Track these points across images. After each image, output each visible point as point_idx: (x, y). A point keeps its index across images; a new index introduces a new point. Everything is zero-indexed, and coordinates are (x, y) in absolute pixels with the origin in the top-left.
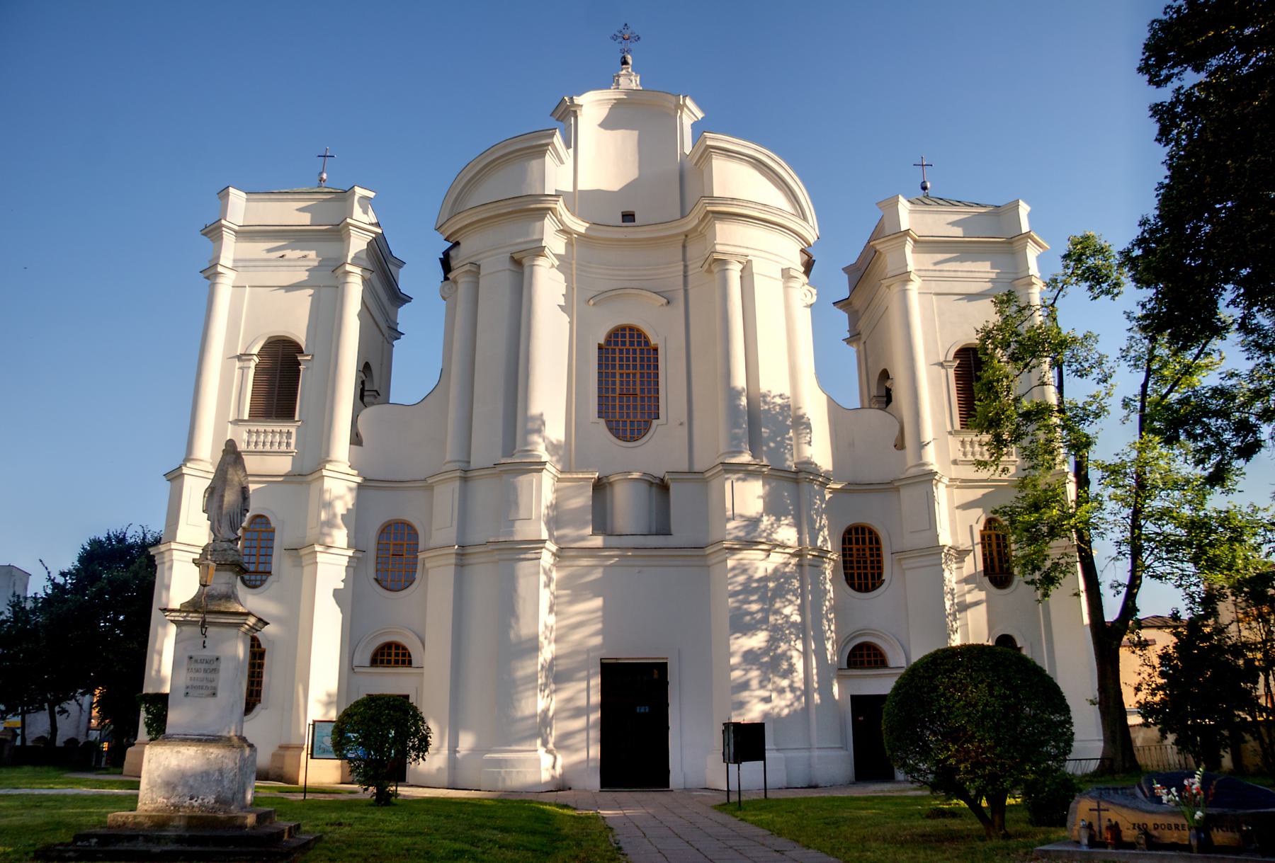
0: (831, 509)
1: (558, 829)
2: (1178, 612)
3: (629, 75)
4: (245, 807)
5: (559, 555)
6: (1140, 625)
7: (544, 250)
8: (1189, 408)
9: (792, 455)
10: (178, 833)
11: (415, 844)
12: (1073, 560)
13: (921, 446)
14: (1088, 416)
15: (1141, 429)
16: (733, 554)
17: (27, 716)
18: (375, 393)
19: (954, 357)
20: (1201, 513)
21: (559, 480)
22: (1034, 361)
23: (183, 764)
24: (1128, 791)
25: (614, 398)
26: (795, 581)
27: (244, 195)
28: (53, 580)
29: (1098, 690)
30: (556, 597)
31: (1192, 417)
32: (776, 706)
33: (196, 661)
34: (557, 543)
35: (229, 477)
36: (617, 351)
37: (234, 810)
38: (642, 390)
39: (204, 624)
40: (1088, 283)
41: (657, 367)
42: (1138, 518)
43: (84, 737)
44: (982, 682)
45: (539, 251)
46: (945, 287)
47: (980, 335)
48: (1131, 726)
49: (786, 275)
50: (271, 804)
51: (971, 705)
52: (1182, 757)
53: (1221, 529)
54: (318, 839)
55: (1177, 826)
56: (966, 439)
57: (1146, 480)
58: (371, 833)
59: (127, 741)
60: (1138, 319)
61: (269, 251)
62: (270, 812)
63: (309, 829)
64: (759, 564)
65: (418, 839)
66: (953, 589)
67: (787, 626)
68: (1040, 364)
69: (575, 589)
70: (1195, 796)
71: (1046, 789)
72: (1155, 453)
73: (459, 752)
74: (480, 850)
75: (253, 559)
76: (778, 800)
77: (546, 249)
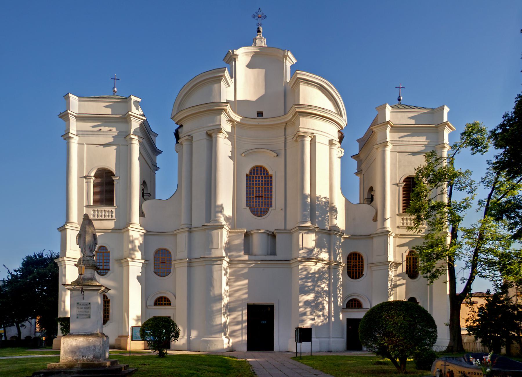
0: (343, 246)
1: (231, 366)
2: (490, 291)
3: (261, 38)
4: (106, 359)
5: (230, 263)
6: (471, 295)
7: (221, 130)
8: (510, 205)
9: (328, 223)
10: (78, 370)
11: (175, 371)
12: (445, 268)
13: (385, 220)
14: (461, 208)
15: (485, 214)
16: (302, 263)
17: (6, 328)
18: (149, 194)
19: (403, 181)
20: (507, 251)
21: (230, 232)
22: (440, 183)
23: (78, 344)
24: (458, 359)
25: (253, 198)
26: (327, 274)
27: (77, 98)
28: (11, 273)
29: (450, 320)
30: (229, 279)
31: (511, 209)
32: (317, 322)
33: (80, 305)
34: (229, 258)
35: (87, 230)
36: (254, 177)
37: (101, 361)
38: (265, 195)
39: (82, 290)
40: (472, 147)
41: (271, 185)
42: (477, 252)
43: (34, 335)
44: (400, 315)
45: (219, 130)
46: (403, 149)
47: (417, 171)
48: (462, 335)
49: (331, 143)
50: (117, 358)
51: (395, 323)
52: (483, 348)
53: (515, 258)
54: (136, 370)
55: (478, 374)
56: (404, 217)
57: (483, 236)
58: (157, 368)
59: (53, 336)
60: (493, 164)
61: (93, 127)
62: (116, 361)
63: (132, 367)
64: (312, 267)
65: (176, 369)
66: (392, 279)
67: (322, 292)
68: (442, 185)
69: (236, 276)
70: (488, 363)
71: (424, 356)
72: (490, 225)
73: (191, 337)
74: (200, 373)
75: (101, 264)
76: (316, 356)
77: (222, 129)
